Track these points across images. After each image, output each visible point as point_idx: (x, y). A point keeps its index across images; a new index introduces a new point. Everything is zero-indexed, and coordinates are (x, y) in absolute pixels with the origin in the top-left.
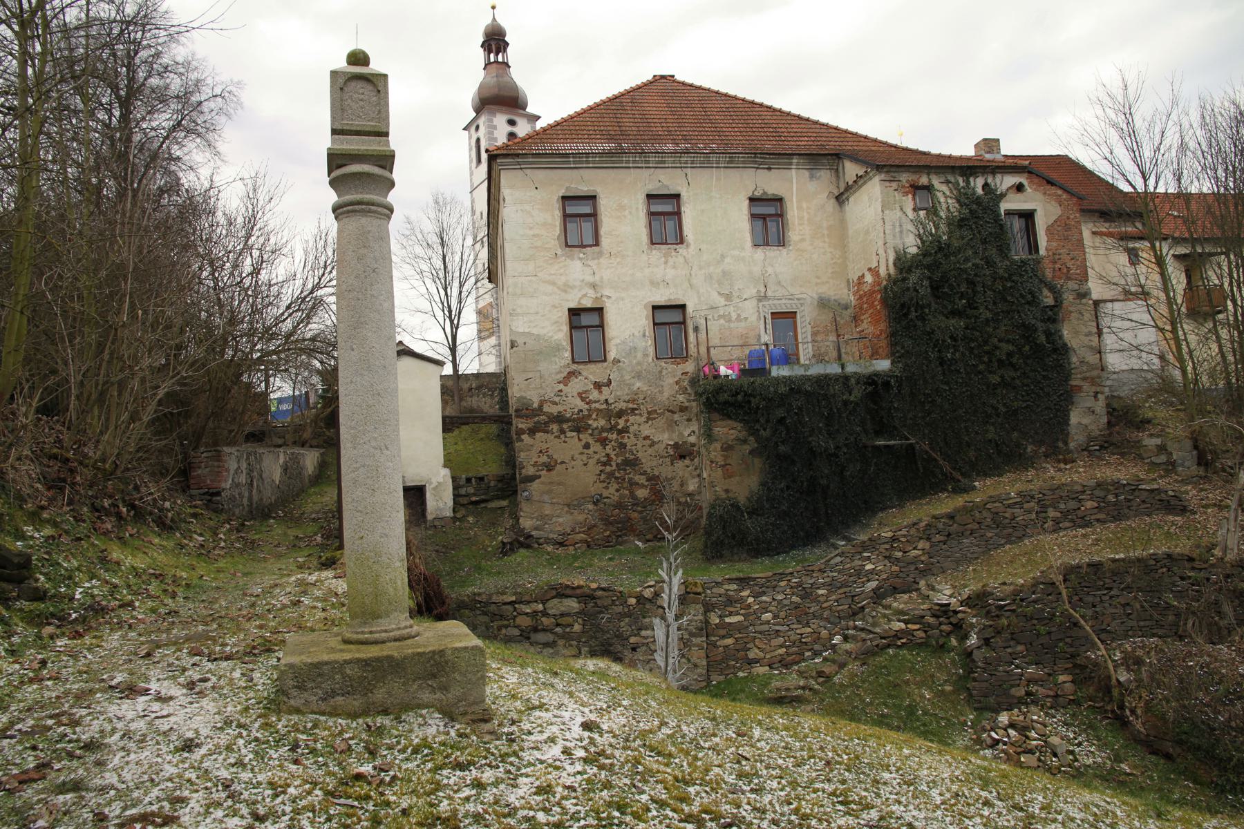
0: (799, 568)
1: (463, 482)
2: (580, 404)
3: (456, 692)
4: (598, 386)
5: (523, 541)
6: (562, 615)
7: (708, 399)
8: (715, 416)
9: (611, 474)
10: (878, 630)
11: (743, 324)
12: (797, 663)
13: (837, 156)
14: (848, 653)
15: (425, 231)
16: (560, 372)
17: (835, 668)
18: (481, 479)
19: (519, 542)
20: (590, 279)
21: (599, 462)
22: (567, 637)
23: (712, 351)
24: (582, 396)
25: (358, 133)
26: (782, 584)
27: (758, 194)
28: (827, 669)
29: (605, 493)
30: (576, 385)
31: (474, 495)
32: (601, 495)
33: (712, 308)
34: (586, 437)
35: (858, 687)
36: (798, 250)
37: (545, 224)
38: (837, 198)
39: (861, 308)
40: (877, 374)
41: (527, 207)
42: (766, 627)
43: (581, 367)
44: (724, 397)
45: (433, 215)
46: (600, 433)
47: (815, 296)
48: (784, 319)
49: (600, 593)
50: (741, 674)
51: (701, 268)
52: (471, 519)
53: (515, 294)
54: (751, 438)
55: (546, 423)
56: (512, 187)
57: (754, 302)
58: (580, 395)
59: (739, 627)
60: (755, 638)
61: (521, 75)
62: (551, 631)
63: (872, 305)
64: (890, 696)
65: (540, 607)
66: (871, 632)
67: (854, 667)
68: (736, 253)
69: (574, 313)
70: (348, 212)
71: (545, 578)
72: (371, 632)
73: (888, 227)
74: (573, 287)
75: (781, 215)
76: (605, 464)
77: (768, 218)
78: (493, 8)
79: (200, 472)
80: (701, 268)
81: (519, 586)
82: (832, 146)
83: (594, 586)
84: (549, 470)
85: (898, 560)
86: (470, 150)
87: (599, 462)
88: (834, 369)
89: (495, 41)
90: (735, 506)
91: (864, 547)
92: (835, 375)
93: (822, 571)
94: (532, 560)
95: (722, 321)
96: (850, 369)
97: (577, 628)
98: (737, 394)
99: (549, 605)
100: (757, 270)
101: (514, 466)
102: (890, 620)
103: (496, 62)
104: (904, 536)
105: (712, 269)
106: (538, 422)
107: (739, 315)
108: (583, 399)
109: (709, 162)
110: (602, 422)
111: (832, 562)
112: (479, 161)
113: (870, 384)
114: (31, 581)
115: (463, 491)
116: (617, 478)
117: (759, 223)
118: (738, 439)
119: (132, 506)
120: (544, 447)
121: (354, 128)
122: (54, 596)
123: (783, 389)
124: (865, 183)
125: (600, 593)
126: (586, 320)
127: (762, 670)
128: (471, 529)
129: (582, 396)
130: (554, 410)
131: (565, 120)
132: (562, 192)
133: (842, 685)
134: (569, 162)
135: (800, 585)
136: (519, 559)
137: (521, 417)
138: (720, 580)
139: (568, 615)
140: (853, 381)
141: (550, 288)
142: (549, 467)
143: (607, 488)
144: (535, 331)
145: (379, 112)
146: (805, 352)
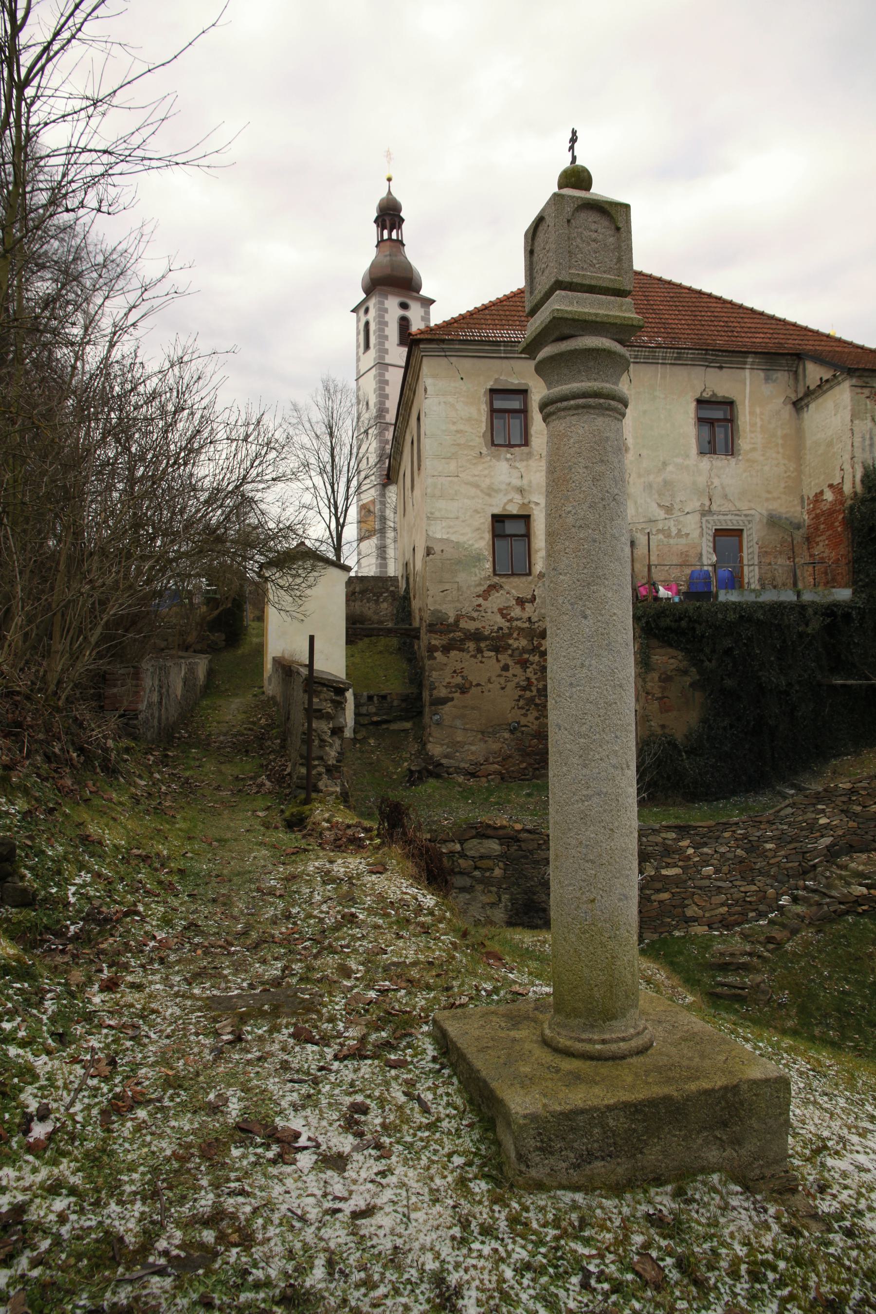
0: (744, 818)
1: (364, 700)
2: (499, 619)
3: (751, 1146)
4: (521, 602)
5: (432, 770)
6: (482, 857)
7: (647, 623)
8: (654, 642)
9: (531, 700)
10: (834, 893)
11: (683, 541)
12: (739, 924)
13: (798, 357)
14: (802, 918)
15: (314, 420)
16: (480, 585)
17: (786, 933)
18: (384, 697)
19: (428, 771)
20: (517, 482)
21: (518, 686)
22: (486, 882)
23: (653, 569)
24: (503, 612)
25: (592, 289)
26: (727, 835)
27: (706, 395)
28: (778, 933)
29: (523, 721)
30: (497, 600)
31: (376, 714)
32: (518, 723)
33: (651, 521)
34: (505, 658)
35: (814, 958)
36: (748, 460)
37: (469, 419)
38: (795, 404)
39: (817, 529)
40: (836, 604)
41: (450, 399)
42: (706, 882)
43: (504, 580)
44: (666, 622)
45: (321, 403)
46: (521, 654)
47: (765, 513)
48: (728, 538)
49: (525, 835)
50: (677, 933)
51: (639, 476)
52: (372, 741)
53: (433, 496)
54: (693, 669)
55: (462, 641)
56: (434, 376)
57: (697, 516)
58: (500, 610)
59: (676, 881)
60: (694, 894)
61: (417, 254)
62: (468, 874)
63: (831, 526)
64: (852, 971)
65: (458, 847)
66: (825, 895)
67: (808, 934)
68: (679, 460)
69: (498, 520)
70: (577, 407)
71: (462, 814)
72: (604, 1042)
73: (858, 440)
74: (497, 491)
75: (730, 421)
76: (524, 689)
77: (717, 424)
78: (389, 180)
79: (115, 690)
80: (639, 476)
81: (434, 822)
82: (792, 344)
83: (518, 827)
84: (463, 693)
85: (856, 815)
86: (358, 334)
87: (518, 686)
88: (788, 596)
89: (389, 216)
90: (672, 744)
91: (819, 798)
92: (790, 603)
93: (770, 823)
94: (444, 792)
95: (661, 536)
96: (807, 597)
97: (498, 872)
98: (681, 619)
99: (467, 845)
100: (702, 480)
101: (420, 685)
102: (848, 884)
103: (390, 239)
104: (865, 788)
105: (651, 477)
106: (453, 639)
107: (679, 530)
108: (504, 616)
109: (654, 358)
110: (523, 642)
111: (782, 813)
112: (367, 346)
113: (828, 616)
114: (16, 879)
115: (364, 710)
116: (537, 705)
117: (706, 429)
118: (677, 670)
119: (81, 750)
120: (459, 666)
121: (587, 282)
122: (45, 900)
123: (732, 617)
124: (831, 388)
125: (525, 835)
126: (511, 528)
127: (700, 930)
128: (372, 752)
129: (503, 612)
130: (471, 626)
131: (493, 304)
132: (490, 385)
133: (794, 954)
134: (499, 351)
135: (745, 837)
136: (430, 791)
137: (435, 632)
138: (657, 826)
139: (489, 857)
140: (810, 611)
141: (473, 491)
142: (463, 689)
143: (525, 715)
144: (454, 538)
145: (619, 260)
146: (751, 575)
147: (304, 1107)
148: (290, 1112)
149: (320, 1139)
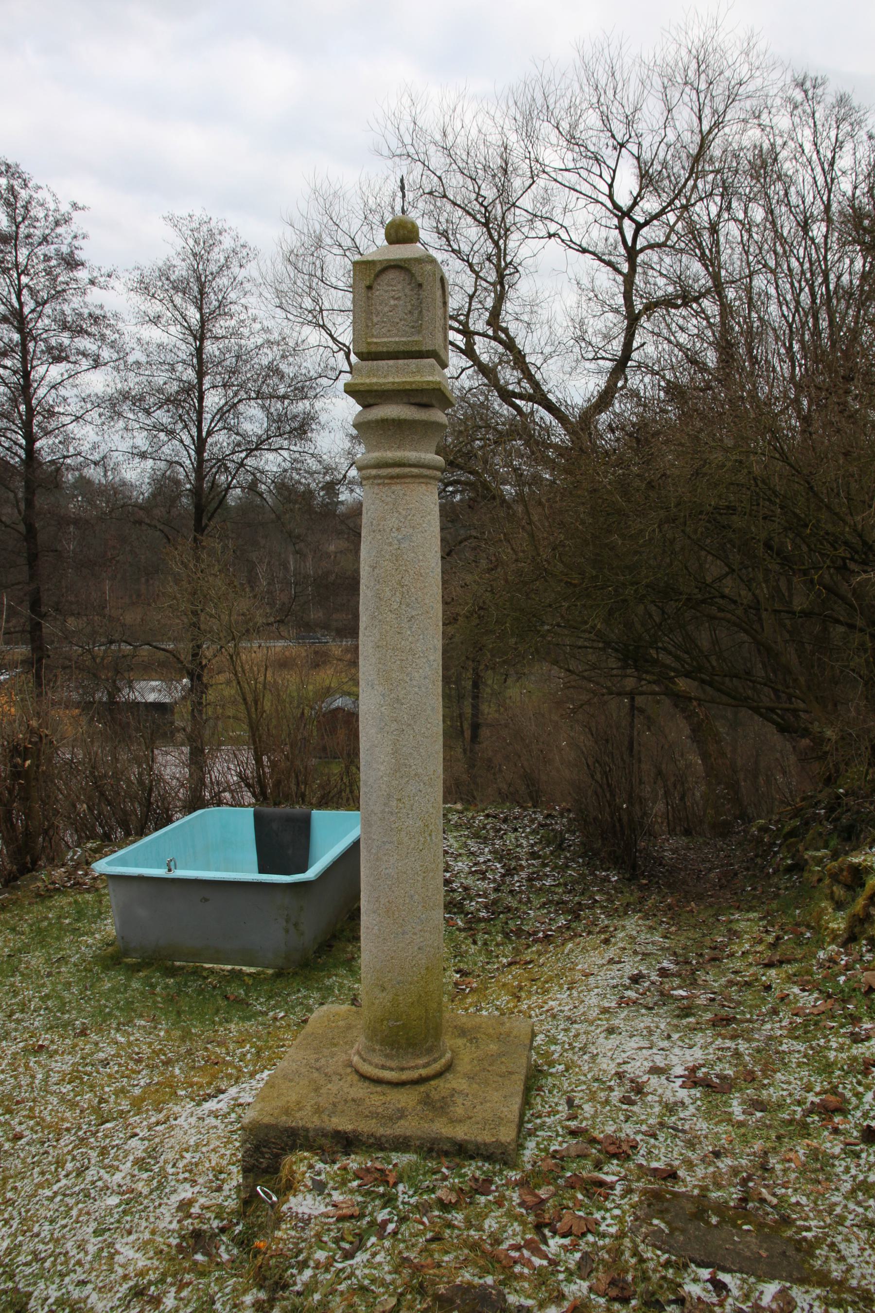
147: (675, 1103)
148: (687, 1101)
149: (665, 1082)
